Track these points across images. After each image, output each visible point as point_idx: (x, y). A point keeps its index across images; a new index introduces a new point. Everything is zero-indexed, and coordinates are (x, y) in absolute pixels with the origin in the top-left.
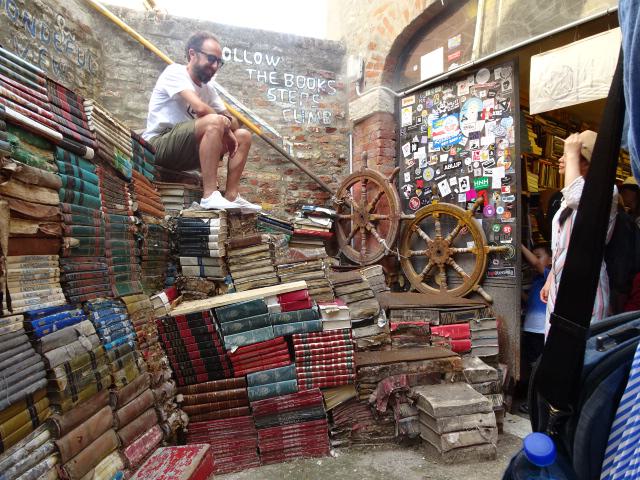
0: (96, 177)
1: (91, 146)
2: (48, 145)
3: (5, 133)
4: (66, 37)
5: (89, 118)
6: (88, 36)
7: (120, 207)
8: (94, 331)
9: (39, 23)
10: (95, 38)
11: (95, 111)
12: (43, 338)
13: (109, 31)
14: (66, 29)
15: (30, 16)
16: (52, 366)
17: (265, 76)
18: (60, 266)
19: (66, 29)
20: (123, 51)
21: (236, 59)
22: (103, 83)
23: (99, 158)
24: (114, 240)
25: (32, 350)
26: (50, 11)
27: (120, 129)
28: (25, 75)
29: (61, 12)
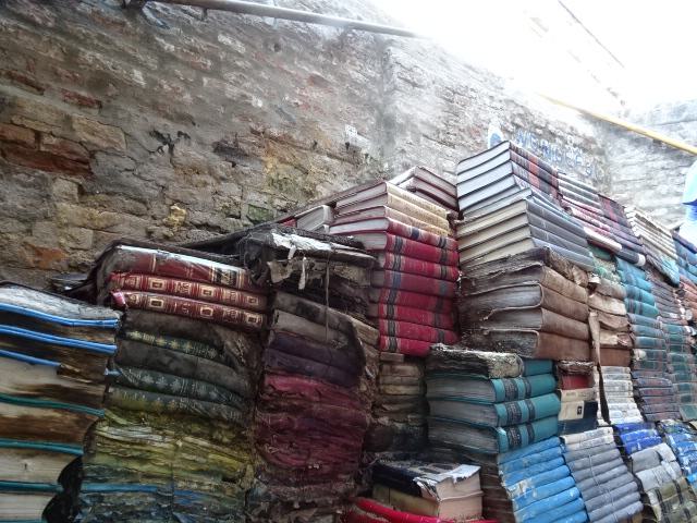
0: (649, 285)
1: (642, 253)
2: (607, 256)
3: (587, 250)
5: (632, 224)
6: (593, 146)
7: (674, 316)
8: (674, 458)
9: (554, 147)
10: (599, 145)
11: (637, 216)
12: (632, 456)
13: (612, 136)
14: (575, 146)
15: (546, 142)
16: (646, 489)
18: (633, 379)
19: (575, 146)
20: (629, 150)
22: (610, 187)
23: (651, 267)
24: (673, 354)
25: (624, 468)
26: (561, 133)
27: (660, 231)
28: (585, 195)
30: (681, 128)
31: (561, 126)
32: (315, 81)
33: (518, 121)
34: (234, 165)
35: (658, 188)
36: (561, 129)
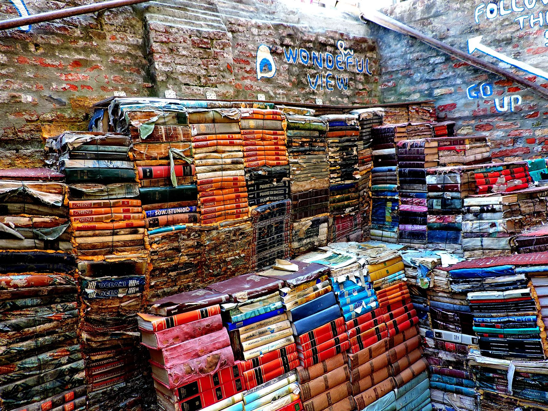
4: (346, 55)
17: (541, 19)
21: (503, 12)
29: (341, 38)
30: (10, 339)
31: (331, 35)
32: (77, 63)
33: (287, 41)
34: (17, 151)
35: (414, 77)
36: (332, 38)
